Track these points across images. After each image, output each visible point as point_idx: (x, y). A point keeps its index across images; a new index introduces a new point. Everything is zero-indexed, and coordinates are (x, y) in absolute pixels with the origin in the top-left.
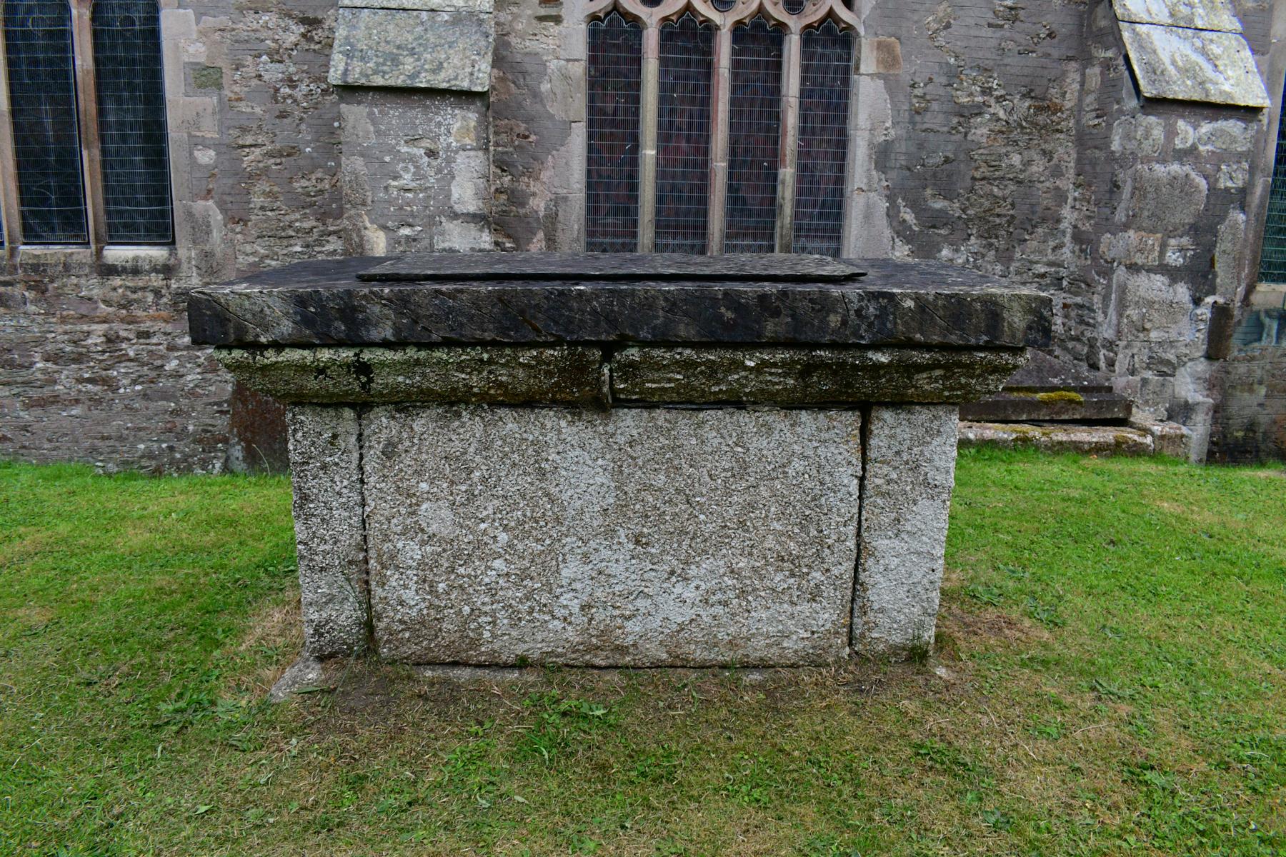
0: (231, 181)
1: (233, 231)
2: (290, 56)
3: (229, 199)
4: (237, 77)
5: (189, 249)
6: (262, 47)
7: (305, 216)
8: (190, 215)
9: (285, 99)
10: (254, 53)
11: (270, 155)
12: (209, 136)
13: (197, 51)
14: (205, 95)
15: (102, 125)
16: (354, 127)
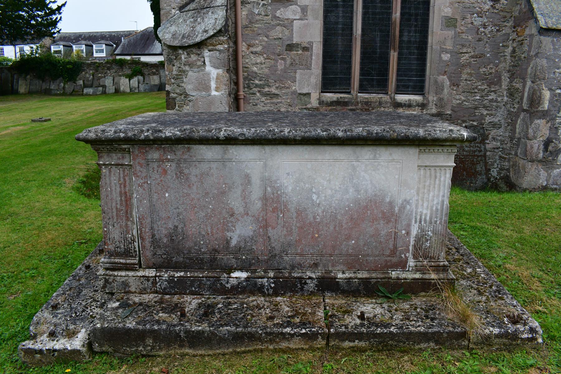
0: (455, 68)
1: (453, 89)
2: (485, 14)
3: (453, 75)
4: (463, 23)
5: (434, 97)
6: (475, 10)
7: (483, 84)
8: (436, 82)
9: (481, 33)
10: (471, 13)
11: (472, 57)
12: (448, 48)
13: (448, 11)
14: (449, 30)
15: (401, 42)
16: (545, 46)
